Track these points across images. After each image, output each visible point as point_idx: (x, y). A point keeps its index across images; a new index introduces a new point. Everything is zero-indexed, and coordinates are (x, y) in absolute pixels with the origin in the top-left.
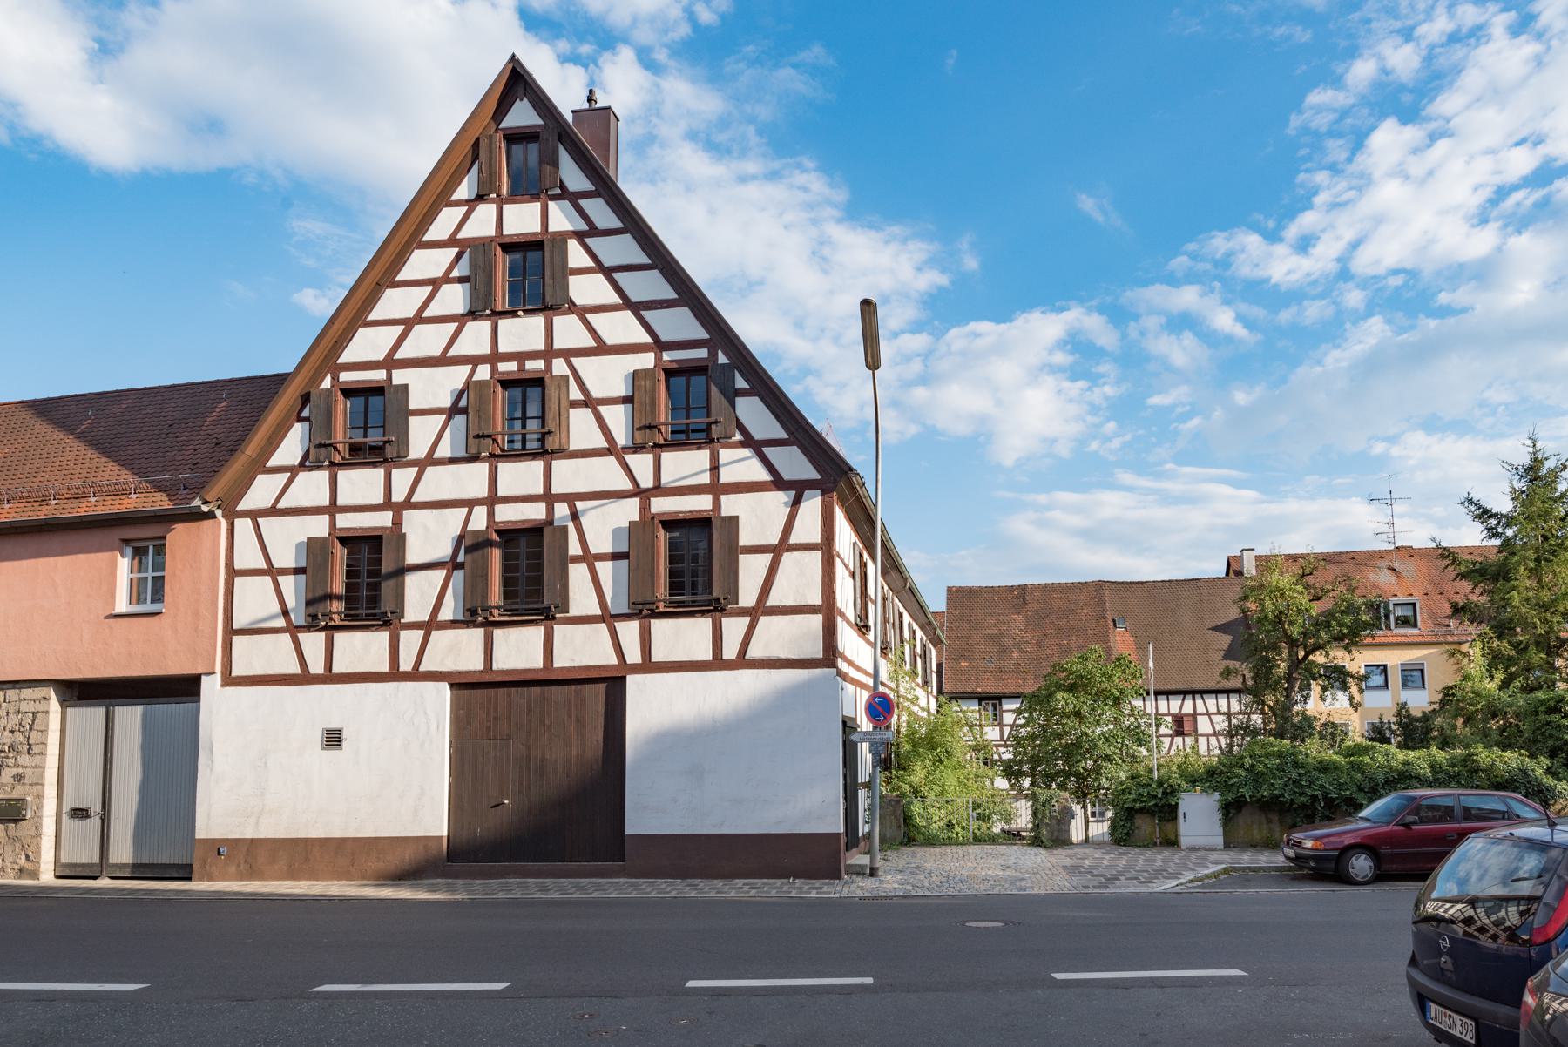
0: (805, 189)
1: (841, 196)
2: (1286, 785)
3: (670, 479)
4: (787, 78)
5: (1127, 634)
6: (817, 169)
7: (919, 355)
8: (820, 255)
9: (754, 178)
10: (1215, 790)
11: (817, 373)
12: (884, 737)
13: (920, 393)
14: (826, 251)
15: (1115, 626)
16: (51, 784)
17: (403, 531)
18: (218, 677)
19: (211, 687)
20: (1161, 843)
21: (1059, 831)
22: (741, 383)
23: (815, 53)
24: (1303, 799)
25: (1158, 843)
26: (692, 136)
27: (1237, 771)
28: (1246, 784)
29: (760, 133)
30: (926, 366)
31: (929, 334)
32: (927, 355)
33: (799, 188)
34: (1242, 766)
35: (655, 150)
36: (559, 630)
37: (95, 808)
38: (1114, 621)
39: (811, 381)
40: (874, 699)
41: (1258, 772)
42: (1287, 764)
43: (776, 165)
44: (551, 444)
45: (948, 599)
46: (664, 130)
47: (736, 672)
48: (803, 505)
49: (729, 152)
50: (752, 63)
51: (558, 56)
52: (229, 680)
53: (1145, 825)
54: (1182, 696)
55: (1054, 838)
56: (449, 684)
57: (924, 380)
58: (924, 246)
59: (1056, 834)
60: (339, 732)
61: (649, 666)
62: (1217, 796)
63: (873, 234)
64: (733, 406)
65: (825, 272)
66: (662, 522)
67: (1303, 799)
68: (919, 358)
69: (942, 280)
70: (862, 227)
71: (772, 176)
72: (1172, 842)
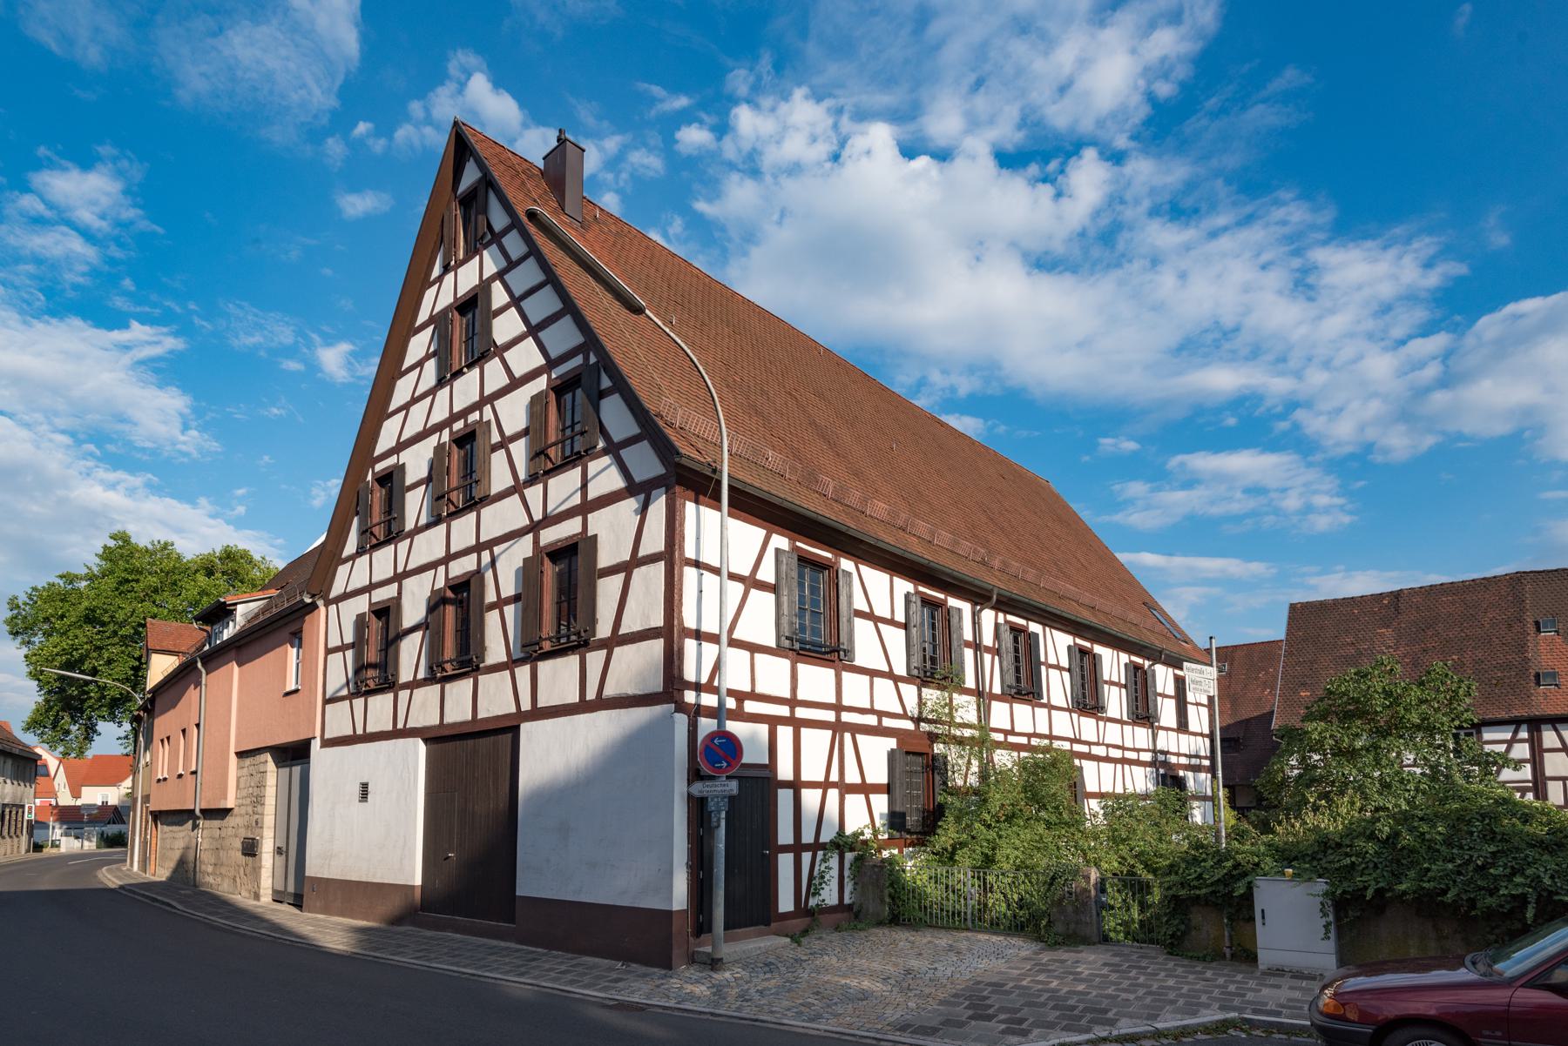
0: (1284, 223)
1: (1327, 216)
2: (1459, 873)
3: (554, 506)
4: (1260, 116)
5: (1559, 640)
6: (1299, 198)
7: (1434, 358)
8: (1304, 284)
9: (1226, 229)
10: (1320, 877)
11: (1307, 404)
12: (726, 788)
13: (1440, 398)
14: (1311, 280)
15: (1538, 630)
16: (269, 828)
17: (1275, 630)
18: (318, 739)
19: (316, 745)
20: (1233, 956)
21: (1077, 923)
22: (606, 382)
23: (1290, 77)
24: (1489, 901)
25: (1228, 955)
26: (1154, 212)
27: (1360, 843)
28: (1376, 867)
29: (1228, 181)
30: (1447, 366)
31: (1448, 332)
32: (1447, 356)
33: (1277, 223)
34: (1372, 837)
35: (1124, 236)
36: (483, 679)
37: (284, 849)
38: (1537, 624)
39: (1300, 415)
40: (713, 739)
41: (1403, 848)
42: (1472, 833)
43: (1248, 209)
44: (478, 493)
45: (1290, 618)
46: (1129, 214)
47: (595, 714)
48: (651, 509)
49: (1196, 211)
50: (1215, 115)
51: (1029, 180)
52: (327, 743)
53: (1208, 926)
54: (1513, 727)
55: (1071, 932)
56: (423, 740)
57: (1445, 382)
58: (1427, 240)
59: (1072, 926)
60: (367, 784)
61: (538, 713)
62: (1321, 885)
63: (1369, 244)
64: (597, 410)
65: (1311, 299)
66: (548, 555)
67: (1489, 901)
68: (1436, 362)
69: (1459, 269)
70: (1353, 240)
71: (1247, 221)
72: (1249, 957)
